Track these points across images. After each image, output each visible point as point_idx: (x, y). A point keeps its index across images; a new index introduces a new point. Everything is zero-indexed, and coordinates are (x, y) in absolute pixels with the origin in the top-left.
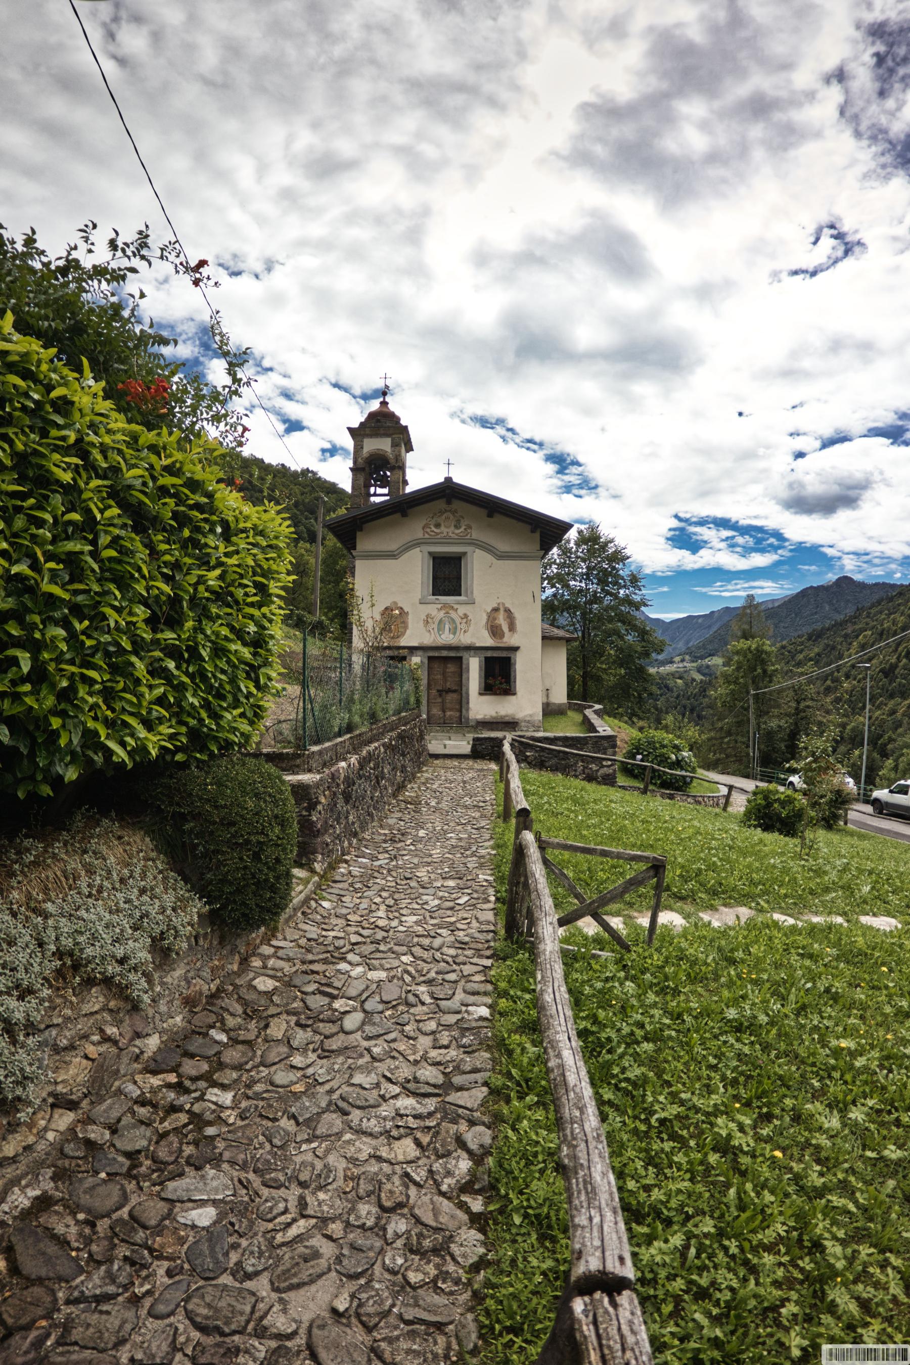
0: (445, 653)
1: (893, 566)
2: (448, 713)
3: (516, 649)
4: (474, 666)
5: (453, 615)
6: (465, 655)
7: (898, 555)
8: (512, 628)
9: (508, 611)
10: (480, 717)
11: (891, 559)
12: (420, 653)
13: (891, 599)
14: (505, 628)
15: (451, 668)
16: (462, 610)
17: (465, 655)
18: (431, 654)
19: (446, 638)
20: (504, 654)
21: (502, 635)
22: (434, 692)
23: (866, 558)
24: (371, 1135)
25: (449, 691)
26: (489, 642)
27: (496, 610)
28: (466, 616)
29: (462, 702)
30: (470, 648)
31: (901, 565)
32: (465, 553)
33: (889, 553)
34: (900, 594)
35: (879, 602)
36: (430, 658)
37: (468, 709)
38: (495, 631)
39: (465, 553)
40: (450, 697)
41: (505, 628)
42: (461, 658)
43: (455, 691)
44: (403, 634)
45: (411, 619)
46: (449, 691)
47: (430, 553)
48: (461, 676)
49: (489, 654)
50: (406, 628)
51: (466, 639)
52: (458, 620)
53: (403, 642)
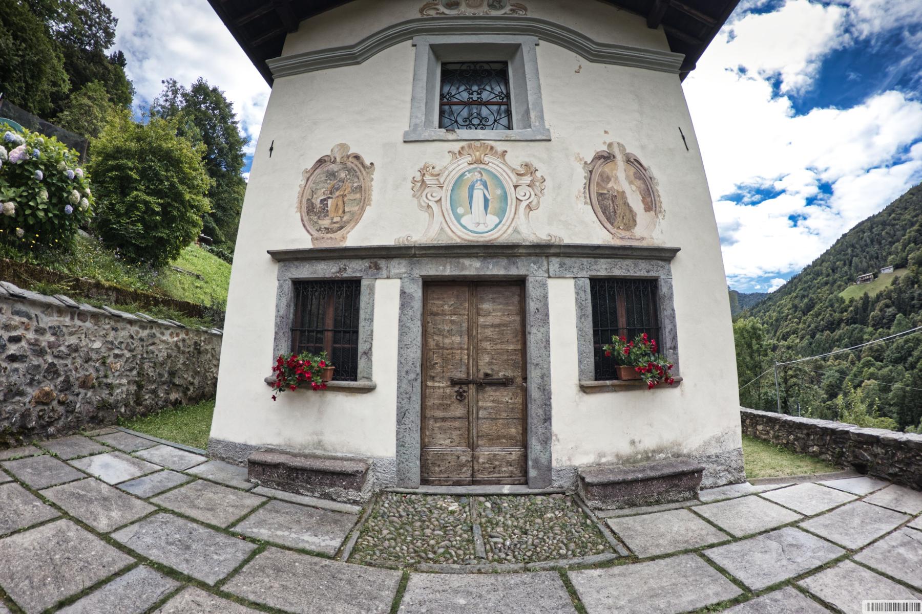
0: (472, 267)
1: (753, 283)
2: (485, 452)
3: (667, 255)
4: (563, 307)
5: (494, 164)
6: (532, 271)
7: (755, 276)
8: (651, 202)
9: (632, 161)
10: (583, 460)
11: (752, 279)
12: (399, 267)
13: (764, 303)
14: (635, 201)
15: (493, 312)
16: (517, 155)
17: (532, 271)
18: (434, 269)
19: (478, 225)
20: (640, 270)
21: (631, 223)
22: (440, 385)
23: (736, 279)
24: (451, 495)
25: (487, 382)
26: (598, 234)
27: (606, 157)
28: (530, 170)
29: (528, 420)
30: (542, 251)
31: (758, 282)
32: (518, 47)
33: (750, 275)
34: (770, 299)
35: (757, 305)
36: (430, 284)
37: (546, 441)
38: (610, 208)
39: (518, 47)
40: (489, 401)
41: (635, 201)
42: (520, 283)
43: (505, 383)
44: (356, 218)
45: (377, 183)
46: (487, 382)
47: (433, 47)
48: (523, 334)
49: (603, 268)
50: (364, 203)
51: (532, 229)
52: (509, 180)
53: (353, 238)
